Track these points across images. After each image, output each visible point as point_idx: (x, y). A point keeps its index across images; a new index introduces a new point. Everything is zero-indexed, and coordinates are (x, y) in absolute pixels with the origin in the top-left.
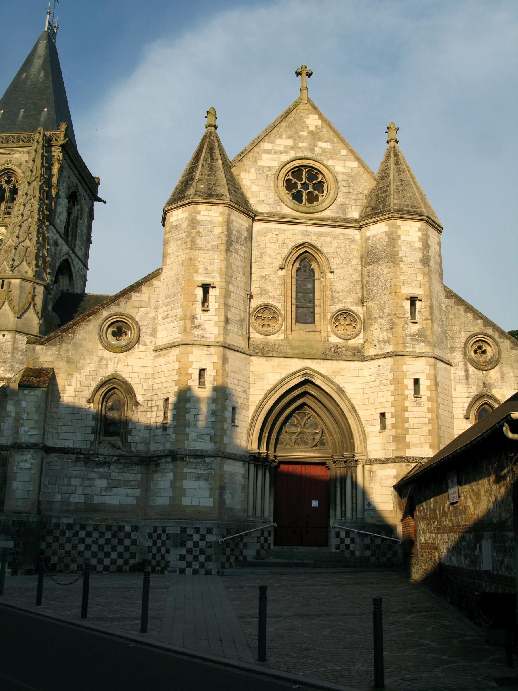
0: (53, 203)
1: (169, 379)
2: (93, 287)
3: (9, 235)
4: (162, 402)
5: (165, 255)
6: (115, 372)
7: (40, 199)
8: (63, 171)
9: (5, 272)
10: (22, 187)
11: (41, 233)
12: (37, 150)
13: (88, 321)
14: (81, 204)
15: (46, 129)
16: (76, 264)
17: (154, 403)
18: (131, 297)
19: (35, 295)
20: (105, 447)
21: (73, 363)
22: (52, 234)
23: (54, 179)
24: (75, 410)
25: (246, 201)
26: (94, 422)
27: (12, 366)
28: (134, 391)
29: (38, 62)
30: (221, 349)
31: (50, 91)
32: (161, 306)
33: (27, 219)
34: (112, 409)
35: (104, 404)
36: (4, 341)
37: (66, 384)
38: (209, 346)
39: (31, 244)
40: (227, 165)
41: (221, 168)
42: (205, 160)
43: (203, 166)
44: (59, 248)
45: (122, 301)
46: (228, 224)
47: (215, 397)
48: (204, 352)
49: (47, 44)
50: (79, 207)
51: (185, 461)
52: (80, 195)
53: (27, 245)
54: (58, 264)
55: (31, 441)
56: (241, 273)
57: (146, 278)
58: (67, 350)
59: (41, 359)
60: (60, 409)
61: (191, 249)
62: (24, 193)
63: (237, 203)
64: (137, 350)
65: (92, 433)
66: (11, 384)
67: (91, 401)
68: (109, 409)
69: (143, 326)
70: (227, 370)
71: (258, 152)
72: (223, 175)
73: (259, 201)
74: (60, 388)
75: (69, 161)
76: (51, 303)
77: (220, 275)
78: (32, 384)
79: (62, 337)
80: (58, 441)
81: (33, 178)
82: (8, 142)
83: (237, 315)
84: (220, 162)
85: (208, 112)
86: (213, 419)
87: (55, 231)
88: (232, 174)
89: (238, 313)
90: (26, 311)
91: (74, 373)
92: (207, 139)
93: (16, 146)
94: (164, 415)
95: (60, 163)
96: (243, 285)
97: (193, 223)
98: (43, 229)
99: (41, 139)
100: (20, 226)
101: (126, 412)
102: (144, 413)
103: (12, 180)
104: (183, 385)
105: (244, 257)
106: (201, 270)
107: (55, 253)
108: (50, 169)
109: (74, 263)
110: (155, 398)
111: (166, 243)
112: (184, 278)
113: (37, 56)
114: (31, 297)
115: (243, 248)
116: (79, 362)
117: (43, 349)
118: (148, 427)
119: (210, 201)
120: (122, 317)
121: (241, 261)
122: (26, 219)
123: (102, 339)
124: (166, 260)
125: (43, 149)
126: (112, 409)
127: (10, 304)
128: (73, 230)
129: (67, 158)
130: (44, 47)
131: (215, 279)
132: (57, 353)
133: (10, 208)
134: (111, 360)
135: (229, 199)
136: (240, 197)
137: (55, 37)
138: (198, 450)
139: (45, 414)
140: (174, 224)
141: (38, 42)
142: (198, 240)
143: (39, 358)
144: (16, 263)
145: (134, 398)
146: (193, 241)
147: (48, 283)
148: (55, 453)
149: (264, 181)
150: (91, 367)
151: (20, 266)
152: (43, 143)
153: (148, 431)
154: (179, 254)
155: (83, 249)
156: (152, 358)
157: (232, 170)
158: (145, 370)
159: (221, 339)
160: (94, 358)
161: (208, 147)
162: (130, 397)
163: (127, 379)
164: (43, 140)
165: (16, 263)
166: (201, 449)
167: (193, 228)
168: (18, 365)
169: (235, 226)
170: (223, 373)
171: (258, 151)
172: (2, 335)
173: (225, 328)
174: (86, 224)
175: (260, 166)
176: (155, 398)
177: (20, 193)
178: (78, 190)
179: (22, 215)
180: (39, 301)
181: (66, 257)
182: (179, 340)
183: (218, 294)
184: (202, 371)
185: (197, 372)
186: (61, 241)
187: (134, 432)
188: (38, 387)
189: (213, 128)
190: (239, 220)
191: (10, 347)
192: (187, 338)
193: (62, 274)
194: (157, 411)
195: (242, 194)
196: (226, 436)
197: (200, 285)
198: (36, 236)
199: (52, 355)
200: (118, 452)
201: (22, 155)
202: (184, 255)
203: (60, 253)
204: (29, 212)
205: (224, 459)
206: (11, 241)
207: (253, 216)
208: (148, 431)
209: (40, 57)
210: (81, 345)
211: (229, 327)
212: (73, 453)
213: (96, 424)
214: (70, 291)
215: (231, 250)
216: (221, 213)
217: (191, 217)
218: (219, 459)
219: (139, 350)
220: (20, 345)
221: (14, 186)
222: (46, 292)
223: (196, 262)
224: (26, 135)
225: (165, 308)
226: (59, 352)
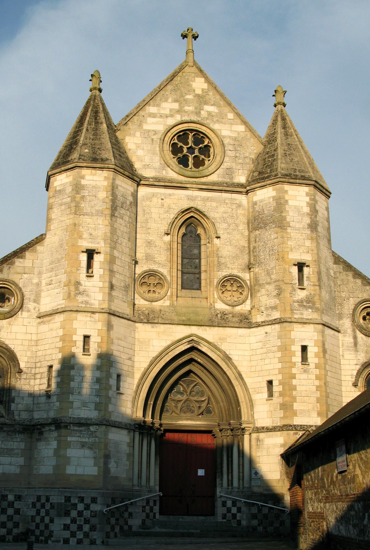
1: (53, 346)
4: (45, 370)
5: (49, 220)
17: (37, 371)
18: (14, 263)
28: (17, 359)
30: (106, 315)
32: (45, 272)
38: (93, 313)
40: (112, 129)
42: (89, 124)
43: (87, 130)
46: (113, 188)
48: (89, 319)
51: (69, 429)
57: (29, 243)
63: (122, 167)
64: (20, 316)
70: (112, 337)
71: (143, 116)
72: (108, 139)
73: (145, 165)
77: (105, 240)
83: (122, 280)
84: (105, 126)
86: (97, 387)
88: (116, 138)
89: (123, 279)
92: (92, 103)
94: (48, 383)
97: (78, 188)
101: (9, 380)
102: (28, 381)
104: (67, 352)
105: (129, 222)
106: (85, 236)
111: (50, 208)
112: (68, 244)
115: (128, 213)
118: (31, 395)
119: (95, 165)
120: (5, 283)
121: (126, 226)
124: (50, 225)
131: (99, 245)
135: (113, 163)
136: (125, 161)
138: (82, 418)
140: (58, 189)
142: (83, 205)
145: (17, 365)
149: (149, 145)
153: (32, 398)
154: (63, 219)
156: (35, 324)
157: (117, 134)
158: (29, 337)
159: (105, 306)
161: (92, 110)
162: (13, 365)
163: (10, 346)
166: (86, 417)
167: (78, 193)
169: (120, 191)
170: (108, 340)
171: (144, 114)
173: (110, 294)
175: (145, 130)
176: (38, 365)
184: (86, 338)
185: (82, 339)
187: (17, 400)
189: (97, 91)
190: (124, 185)
192: (71, 304)
194: (41, 378)
195: (127, 158)
196: (111, 404)
197: (85, 250)
202: (68, 220)
205: (109, 427)
207: (138, 180)
208: (32, 398)
211: (114, 293)
215: (116, 215)
216: (105, 177)
217: (75, 182)
218: (104, 427)
219: (23, 317)
223: (81, 228)
225: (49, 274)
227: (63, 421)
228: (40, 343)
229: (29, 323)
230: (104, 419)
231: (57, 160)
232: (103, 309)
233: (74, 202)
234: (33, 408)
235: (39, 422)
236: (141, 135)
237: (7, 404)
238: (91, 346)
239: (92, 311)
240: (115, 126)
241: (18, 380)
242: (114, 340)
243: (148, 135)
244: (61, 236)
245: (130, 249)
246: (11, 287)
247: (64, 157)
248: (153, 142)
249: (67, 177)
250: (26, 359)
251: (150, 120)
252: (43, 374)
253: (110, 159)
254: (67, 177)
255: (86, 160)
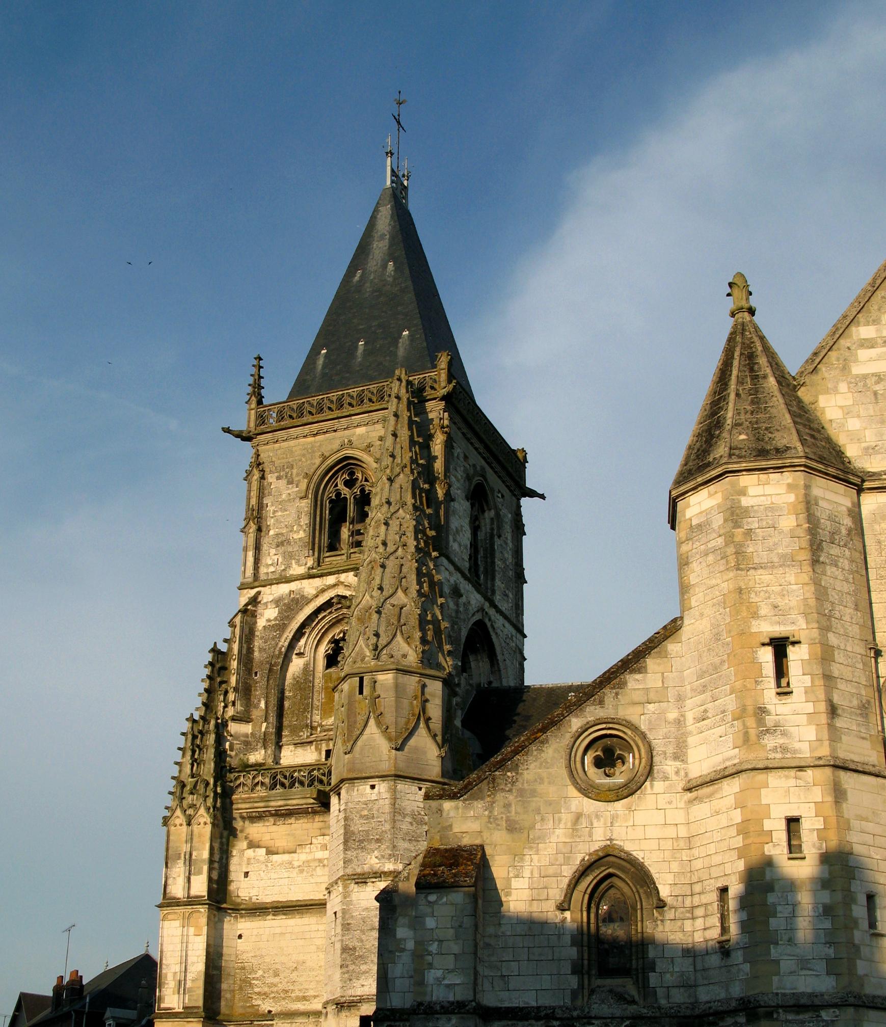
0: (442, 513)
1: (724, 846)
2: (540, 671)
3: (364, 586)
4: (714, 897)
5: (684, 589)
6: (608, 842)
7: (415, 508)
8: (452, 447)
9: (363, 660)
10: (378, 489)
11: (424, 575)
12: (399, 413)
13: (542, 742)
14: (496, 508)
15: (410, 371)
16: (500, 627)
17: (696, 900)
18: (625, 683)
19: (427, 701)
20: (603, 1002)
21: (521, 830)
22: (447, 573)
23: (439, 465)
24: (533, 928)
25: (839, 454)
26: (575, 949)
27: (394, 847)
28: (652, 879)
29: (380, 247)
30: (828, 771)
31: (410, 297)
32: (689, 695)
33: (395, 551)
34: (609, 918)
35: (593, 910)
36: (374, 797)
37: (511, 875)
38: (801, 768)
39: (407, 600)
40: (788, 385)
41: (777, 393)
42: (740, 382)
43: (738, 395)
44: (463, 600)
45: (608, 694)
46: (809, 505)
47: (827, 875)
48: (792, 782)
49: (392, 209)
50: (492, 513)
51: (777, 1019)
52: (492, 490)
53: (401, 603)
54: (464, 633)
55: (451, 999)
56: (850, 605)
57: (650, 640)
58: (507, 806)
59: (456, 829)
60: (503, 928)
61: (738, 569)
62: (384, 501)
63: (821, 460)
64: (649, 791)
65: (573, 973)
66: (400, 884)
67: (566, 906)
68: (604, 921)
69: (657, 739)
70: (846, 816)
71: (849, 348)
72: (783, 406)
73: (867, 449)
74: (500, 885)
75: (462, 425)
76: (459, 713)
77: (805, 615)
78: (444, 881)
79: (494, 779)
80: (505, 995)
81: (398, 470)
82: (362, 402)
83: (852, 695)
84: (772, 381)
85: (731, 285)
86: (827, 924)
87: (451, 568)
88: (799, 401)
89: (854, 691)
90: (411, 734)
91: (526, 851)
92: (739, 339)
93: (357, 411)
94: (722, 924)
95: (446, 433)
96: (858, 631)
97: (735, 514)
98: (427, 566)
99: (403, 391)
100: (383, 566)
101: (639, 924)
102: (679, 923)
103: (357, 479)
104: (754, 856)
105: (851, 572)
106: (764, 610)
107: (457, 612)
108: (428, 447)
109: (496, 626)
110: (697, 888)
111: (683, 563)
112: (730, 631)
113: (376, 236)
114: (419, 705)
115: (847, 553)
116: (532, 827)
117: (457, 808)
118: (690, 953)
119: (764, 464)
120: (611, 726)
121: (847, 580)
122: (392, 550)
123: (576, 776)
124: (689, 599)
125: (409, 410)
126: (609, 918)
127: (379, 724)
128: (486, 562)
129: (458, 419)
130: (389, 217)
131: (796, 625)
132: (487, 813)
133: (359, 533)
134: (597, 817)
135: (802, 454)
136: (824, 447)
137: (407, 194)
138: (803, 994)
139: (475, 940)
140: (694, 523)
141: (376, 211)
142: (750, 550)
143: (451, 826)
144: (383, 641)
145: (654, 892)
146: (739, 553)
147: (450, 673)
148: (500, 1020)
149: (871, 406)
150: (560, 835)
151: (391, 646)
152: (408, 399)
153: (691, 959)
154: (714, 582)
155: (511, 596)
156: (682, 805)
157: (799, 393)
158: (671, 832)
159: (824, 751)
160: (563, 816)
161: (741, 354)
162: (645, 892)
163: (634, 853)
164: (407, 392)
165: (383, 641)
166: (809, 990)
167: (737, 525)
168: (406, 845)
169: (824, 509)
170: (838, 822)
171: (849, 345)
172: (368, 787)
173: (831, 726)
174: (510, 545)
175: (857, 376)
176: (697, 888)
177: (375, 501)
178: (486, 480)
179: (384, 544)
180: (435, 710)
181: (478, 617)
182: (736, 761)
183: (806, 657)
184: (793, 822)
185: (783, 825)
186: (465, 586)
187: (660, 966)
188: (455, 886)
189: (746, 314)
190: (830, 496)
191: (387, 809)
192: (751, 756)
193: (475, 651)
194: (705, 916)
195: (829, 440)
196: (860, 959)
197: (767, 641)
198: (415, 582)
199: (476, 818)
200: (632, 1009)
201: (370, 428)
202: (724, 583)
203: (466, 610)
204: (397, 537)
205: (861, 1010)
206: (367, 597)
207: (855, 481)
208: (691, 959)
209: (382, 237)
210: (533, 793)
211: (839, 723)
212: (538, 1019)
213: (580, 953)
214: (495, 685)
215: (821, 559)
216: (789, 485)
217: (729, 503)
218: (851, 1010)
219: (655, 792)
220: (407, 803)
221: (363, 491)
222: (447, 691)
223: (753, 595)
224: (373, 387)
225: (698, 699)
226: (490, 812)
227: (762, 1003)
228: (696, 842)
229: (670, 803)
230: (850, 992)
231: (686, 465)
232: (820, 758)
233: (732, 545)
234: (695, 980)
235: (710, 1008)
236: (849, 388)
237: (640, 975)
238: (804, 839)
239: (798, 764)
240: (793, 377)
241: (659, 922)
242: (852, 821)
243: (865, 385)
244: (714, 617)
245: (862, 626)
246: (624, 732)
247: (697, 456)
248: (876, 398)
249: (710, 495)
250: (670, 879)
251: (863, 354)
252: (709, 907)
253: (793, 446)
254: (710, 495)
255: (745, 456)
